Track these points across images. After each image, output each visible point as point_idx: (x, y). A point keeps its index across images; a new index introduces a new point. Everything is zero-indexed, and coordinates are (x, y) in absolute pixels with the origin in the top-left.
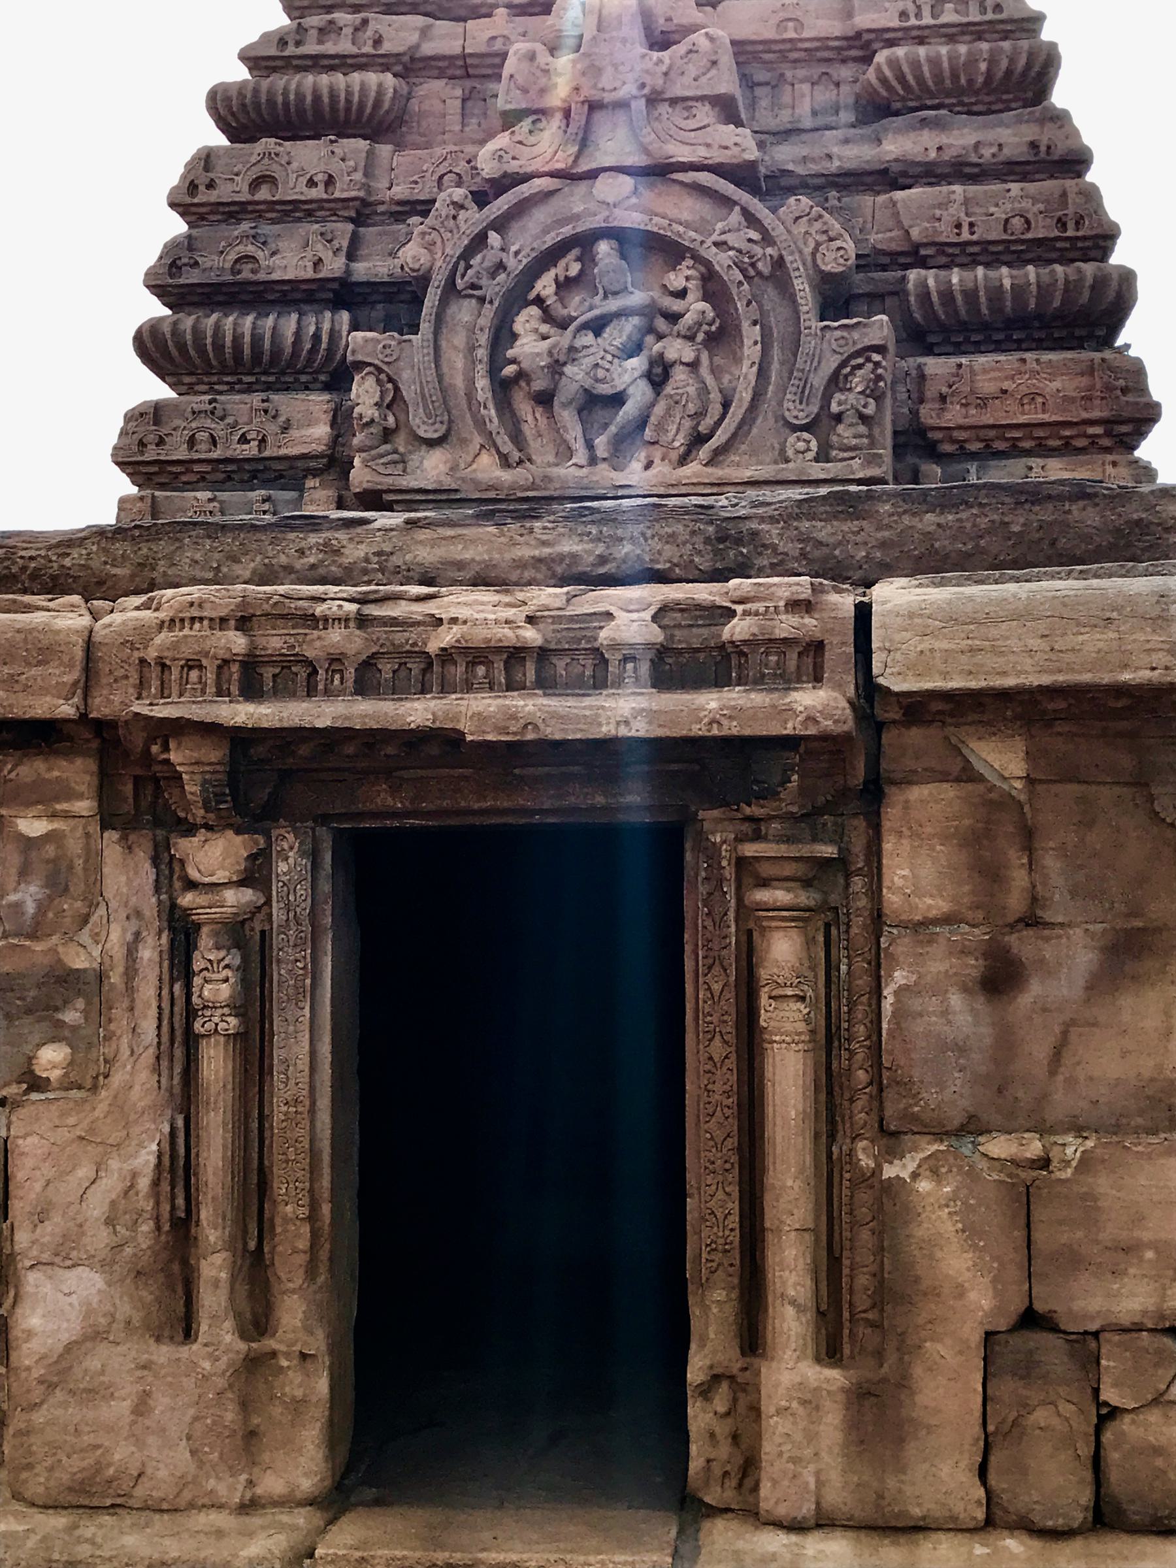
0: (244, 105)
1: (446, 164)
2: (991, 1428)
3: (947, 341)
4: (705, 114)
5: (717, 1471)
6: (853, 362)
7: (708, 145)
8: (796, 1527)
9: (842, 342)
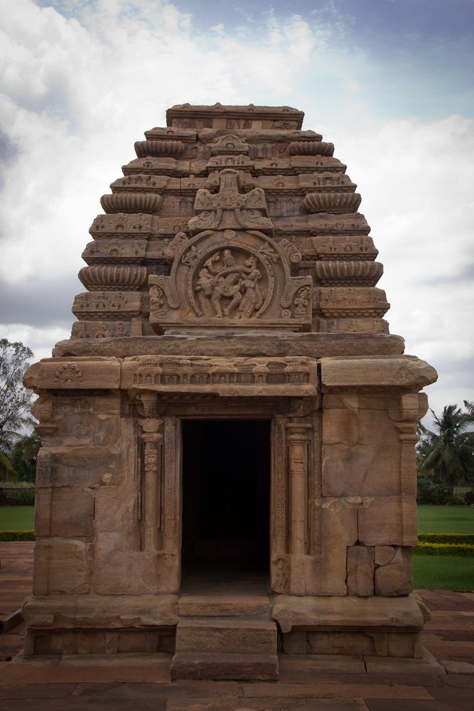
0: (113, 203)
2: (348, 570)
3: (327, 282)
4: (257, 214)
5: (279, 583)
8: (300, 596)
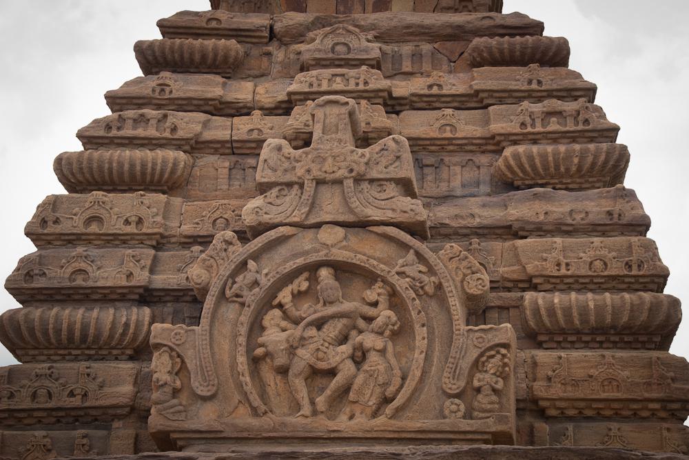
0: (81, 169)
1: (218, 212)
3: (551, 340)
4: (392, 190)
6: (488, 354)
7: (393, 210)
9: (480, 340)
